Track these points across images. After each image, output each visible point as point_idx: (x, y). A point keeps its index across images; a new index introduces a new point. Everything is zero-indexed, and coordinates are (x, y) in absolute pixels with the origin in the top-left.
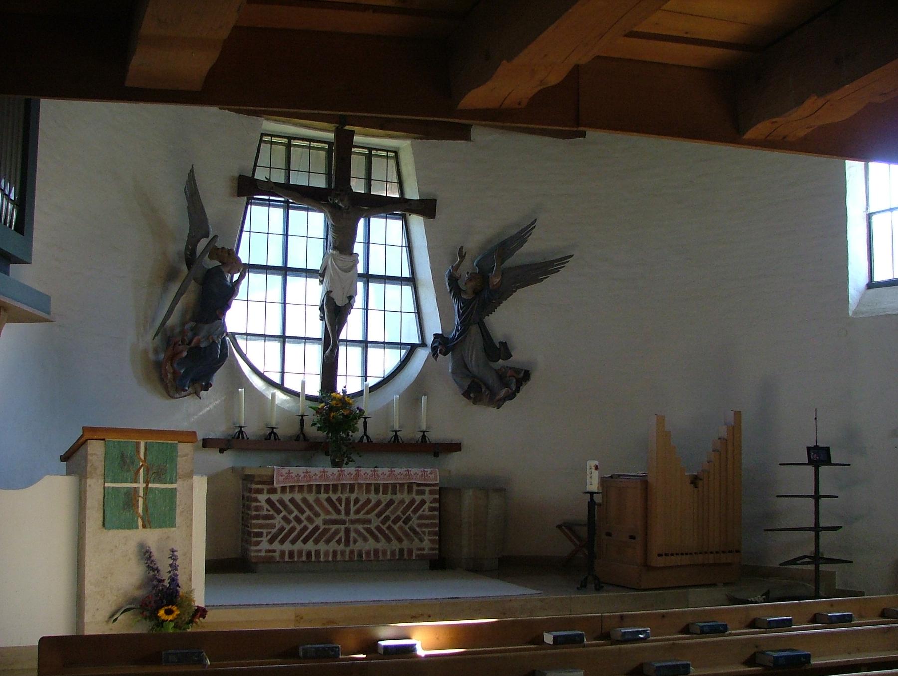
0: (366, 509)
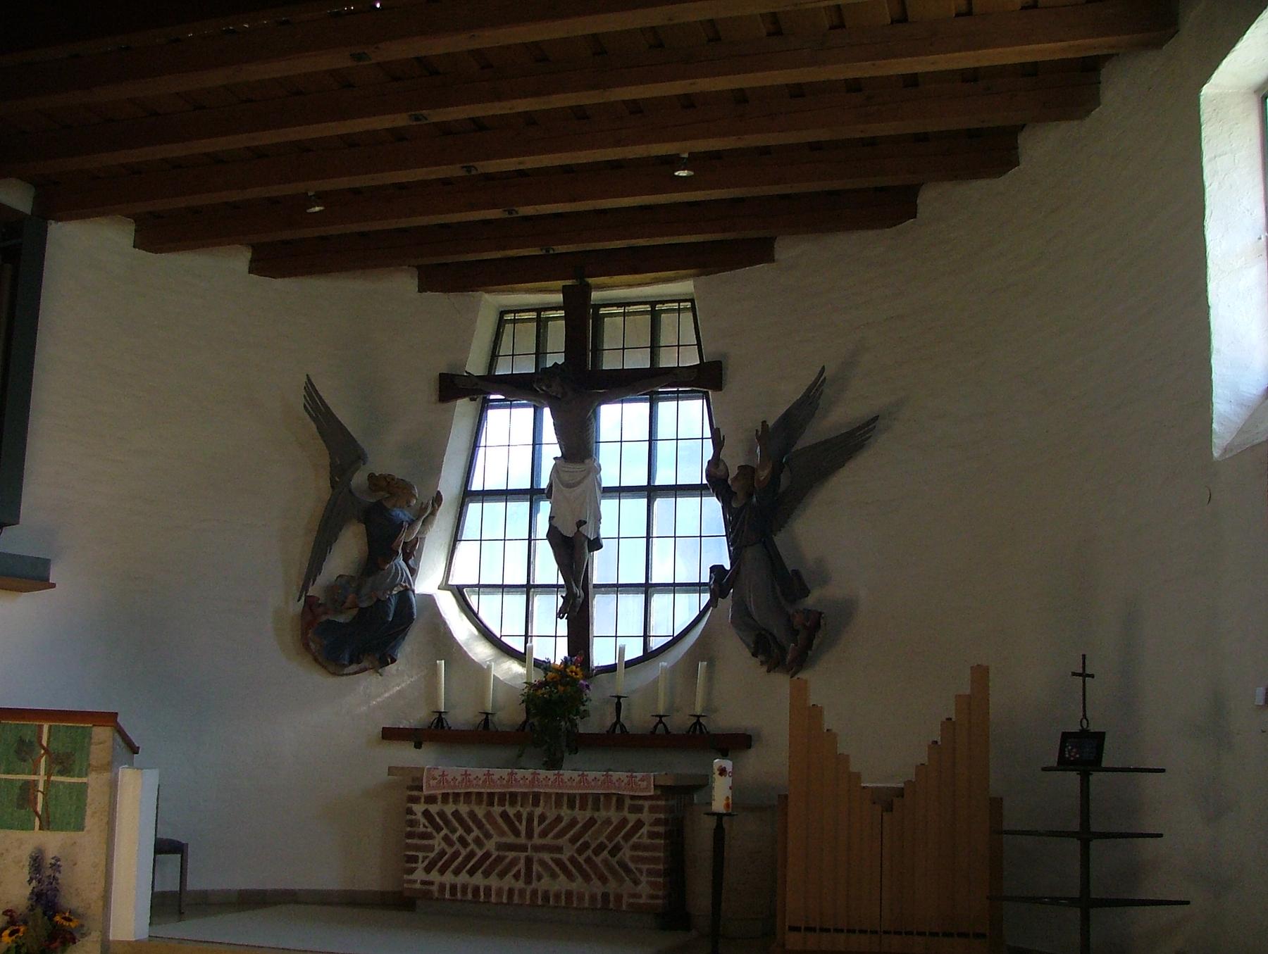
0: (556, 831)
